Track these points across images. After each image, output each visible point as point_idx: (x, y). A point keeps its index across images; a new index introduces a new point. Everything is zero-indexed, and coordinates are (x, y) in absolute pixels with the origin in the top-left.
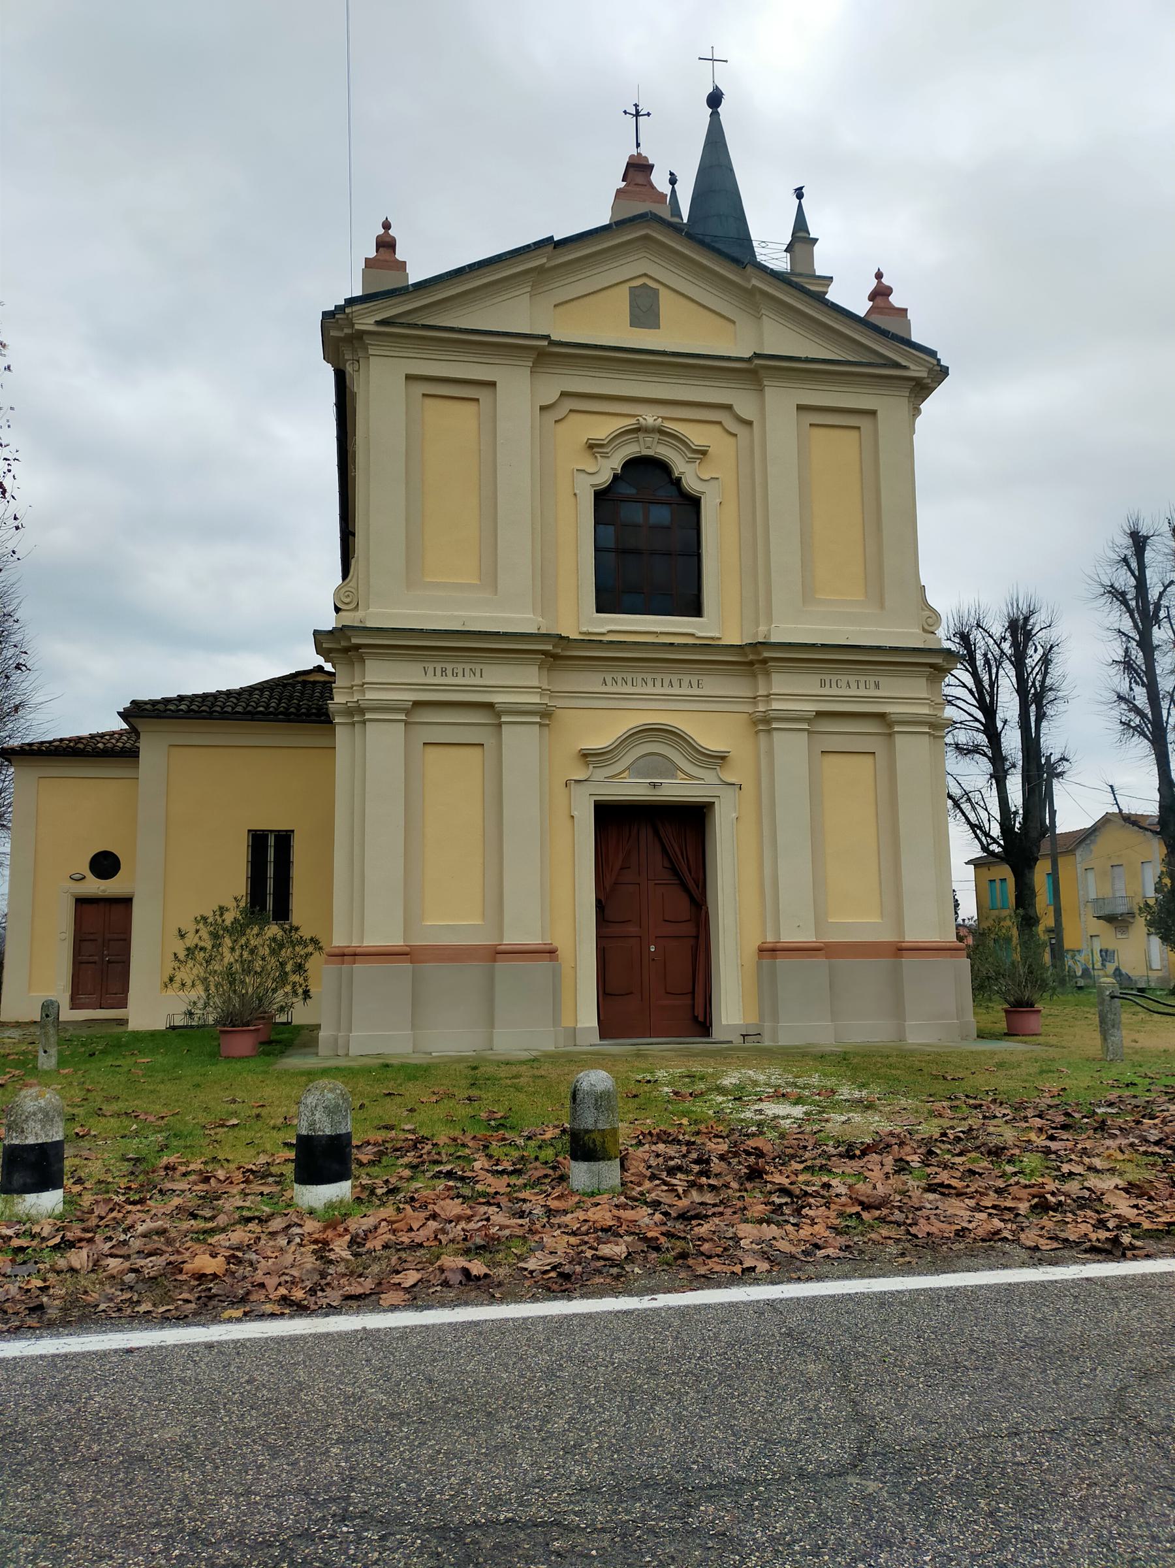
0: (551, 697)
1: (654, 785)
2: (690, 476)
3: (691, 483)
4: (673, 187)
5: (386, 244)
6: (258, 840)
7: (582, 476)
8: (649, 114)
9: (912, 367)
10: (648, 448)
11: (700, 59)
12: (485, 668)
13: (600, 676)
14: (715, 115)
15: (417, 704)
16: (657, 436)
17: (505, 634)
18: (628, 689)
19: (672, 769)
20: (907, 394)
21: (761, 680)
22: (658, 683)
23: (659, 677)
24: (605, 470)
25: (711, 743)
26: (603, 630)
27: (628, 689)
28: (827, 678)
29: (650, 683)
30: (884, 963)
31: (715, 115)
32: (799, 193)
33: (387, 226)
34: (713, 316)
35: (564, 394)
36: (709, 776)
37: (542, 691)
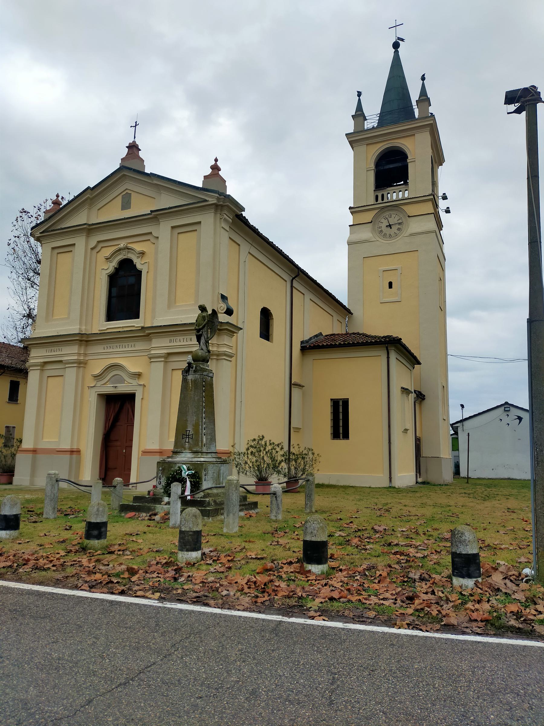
0: (218, 347)
1: (116, 387)
2: (139, 264)
3: (139, 267)
4: (423, 82)
5: (215, 168)
6: (335, 403)
7: (104, 271)
8: (131, 127)
9: (210, 199)
10: (125, 255)
11: (389, 28)
12: (63, 348)
13: (103, 346)
14: (396, 53)
15: (169, 354)
16: (127, 250)
17: (63, 335)
18: (111, 350)
19: (122, 381)
20: (213, 211)
21: (83, 348)
22: (185, 340)
23: (121, 344)
24: (111, 267)
25: (133, 369)
26: (105, 328)
27: (111, 350)
28: (172, 338)
29: (118, 347)
30: (30, 455)
31: (396, 53)
32: (359, 94)
33: (216, 160)
34: (149, 198)
35: (99, 242)
36: (135, 382)
37: (79, 354)
